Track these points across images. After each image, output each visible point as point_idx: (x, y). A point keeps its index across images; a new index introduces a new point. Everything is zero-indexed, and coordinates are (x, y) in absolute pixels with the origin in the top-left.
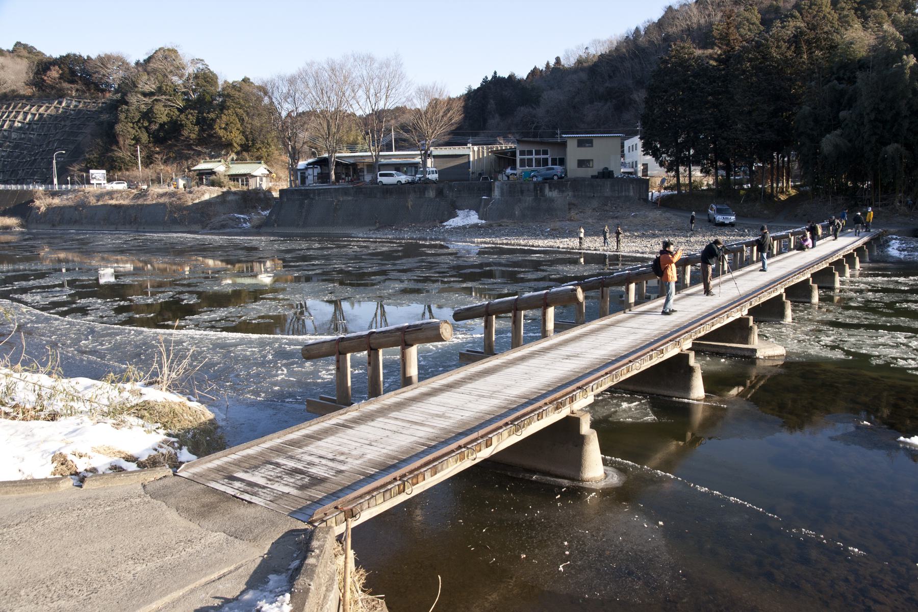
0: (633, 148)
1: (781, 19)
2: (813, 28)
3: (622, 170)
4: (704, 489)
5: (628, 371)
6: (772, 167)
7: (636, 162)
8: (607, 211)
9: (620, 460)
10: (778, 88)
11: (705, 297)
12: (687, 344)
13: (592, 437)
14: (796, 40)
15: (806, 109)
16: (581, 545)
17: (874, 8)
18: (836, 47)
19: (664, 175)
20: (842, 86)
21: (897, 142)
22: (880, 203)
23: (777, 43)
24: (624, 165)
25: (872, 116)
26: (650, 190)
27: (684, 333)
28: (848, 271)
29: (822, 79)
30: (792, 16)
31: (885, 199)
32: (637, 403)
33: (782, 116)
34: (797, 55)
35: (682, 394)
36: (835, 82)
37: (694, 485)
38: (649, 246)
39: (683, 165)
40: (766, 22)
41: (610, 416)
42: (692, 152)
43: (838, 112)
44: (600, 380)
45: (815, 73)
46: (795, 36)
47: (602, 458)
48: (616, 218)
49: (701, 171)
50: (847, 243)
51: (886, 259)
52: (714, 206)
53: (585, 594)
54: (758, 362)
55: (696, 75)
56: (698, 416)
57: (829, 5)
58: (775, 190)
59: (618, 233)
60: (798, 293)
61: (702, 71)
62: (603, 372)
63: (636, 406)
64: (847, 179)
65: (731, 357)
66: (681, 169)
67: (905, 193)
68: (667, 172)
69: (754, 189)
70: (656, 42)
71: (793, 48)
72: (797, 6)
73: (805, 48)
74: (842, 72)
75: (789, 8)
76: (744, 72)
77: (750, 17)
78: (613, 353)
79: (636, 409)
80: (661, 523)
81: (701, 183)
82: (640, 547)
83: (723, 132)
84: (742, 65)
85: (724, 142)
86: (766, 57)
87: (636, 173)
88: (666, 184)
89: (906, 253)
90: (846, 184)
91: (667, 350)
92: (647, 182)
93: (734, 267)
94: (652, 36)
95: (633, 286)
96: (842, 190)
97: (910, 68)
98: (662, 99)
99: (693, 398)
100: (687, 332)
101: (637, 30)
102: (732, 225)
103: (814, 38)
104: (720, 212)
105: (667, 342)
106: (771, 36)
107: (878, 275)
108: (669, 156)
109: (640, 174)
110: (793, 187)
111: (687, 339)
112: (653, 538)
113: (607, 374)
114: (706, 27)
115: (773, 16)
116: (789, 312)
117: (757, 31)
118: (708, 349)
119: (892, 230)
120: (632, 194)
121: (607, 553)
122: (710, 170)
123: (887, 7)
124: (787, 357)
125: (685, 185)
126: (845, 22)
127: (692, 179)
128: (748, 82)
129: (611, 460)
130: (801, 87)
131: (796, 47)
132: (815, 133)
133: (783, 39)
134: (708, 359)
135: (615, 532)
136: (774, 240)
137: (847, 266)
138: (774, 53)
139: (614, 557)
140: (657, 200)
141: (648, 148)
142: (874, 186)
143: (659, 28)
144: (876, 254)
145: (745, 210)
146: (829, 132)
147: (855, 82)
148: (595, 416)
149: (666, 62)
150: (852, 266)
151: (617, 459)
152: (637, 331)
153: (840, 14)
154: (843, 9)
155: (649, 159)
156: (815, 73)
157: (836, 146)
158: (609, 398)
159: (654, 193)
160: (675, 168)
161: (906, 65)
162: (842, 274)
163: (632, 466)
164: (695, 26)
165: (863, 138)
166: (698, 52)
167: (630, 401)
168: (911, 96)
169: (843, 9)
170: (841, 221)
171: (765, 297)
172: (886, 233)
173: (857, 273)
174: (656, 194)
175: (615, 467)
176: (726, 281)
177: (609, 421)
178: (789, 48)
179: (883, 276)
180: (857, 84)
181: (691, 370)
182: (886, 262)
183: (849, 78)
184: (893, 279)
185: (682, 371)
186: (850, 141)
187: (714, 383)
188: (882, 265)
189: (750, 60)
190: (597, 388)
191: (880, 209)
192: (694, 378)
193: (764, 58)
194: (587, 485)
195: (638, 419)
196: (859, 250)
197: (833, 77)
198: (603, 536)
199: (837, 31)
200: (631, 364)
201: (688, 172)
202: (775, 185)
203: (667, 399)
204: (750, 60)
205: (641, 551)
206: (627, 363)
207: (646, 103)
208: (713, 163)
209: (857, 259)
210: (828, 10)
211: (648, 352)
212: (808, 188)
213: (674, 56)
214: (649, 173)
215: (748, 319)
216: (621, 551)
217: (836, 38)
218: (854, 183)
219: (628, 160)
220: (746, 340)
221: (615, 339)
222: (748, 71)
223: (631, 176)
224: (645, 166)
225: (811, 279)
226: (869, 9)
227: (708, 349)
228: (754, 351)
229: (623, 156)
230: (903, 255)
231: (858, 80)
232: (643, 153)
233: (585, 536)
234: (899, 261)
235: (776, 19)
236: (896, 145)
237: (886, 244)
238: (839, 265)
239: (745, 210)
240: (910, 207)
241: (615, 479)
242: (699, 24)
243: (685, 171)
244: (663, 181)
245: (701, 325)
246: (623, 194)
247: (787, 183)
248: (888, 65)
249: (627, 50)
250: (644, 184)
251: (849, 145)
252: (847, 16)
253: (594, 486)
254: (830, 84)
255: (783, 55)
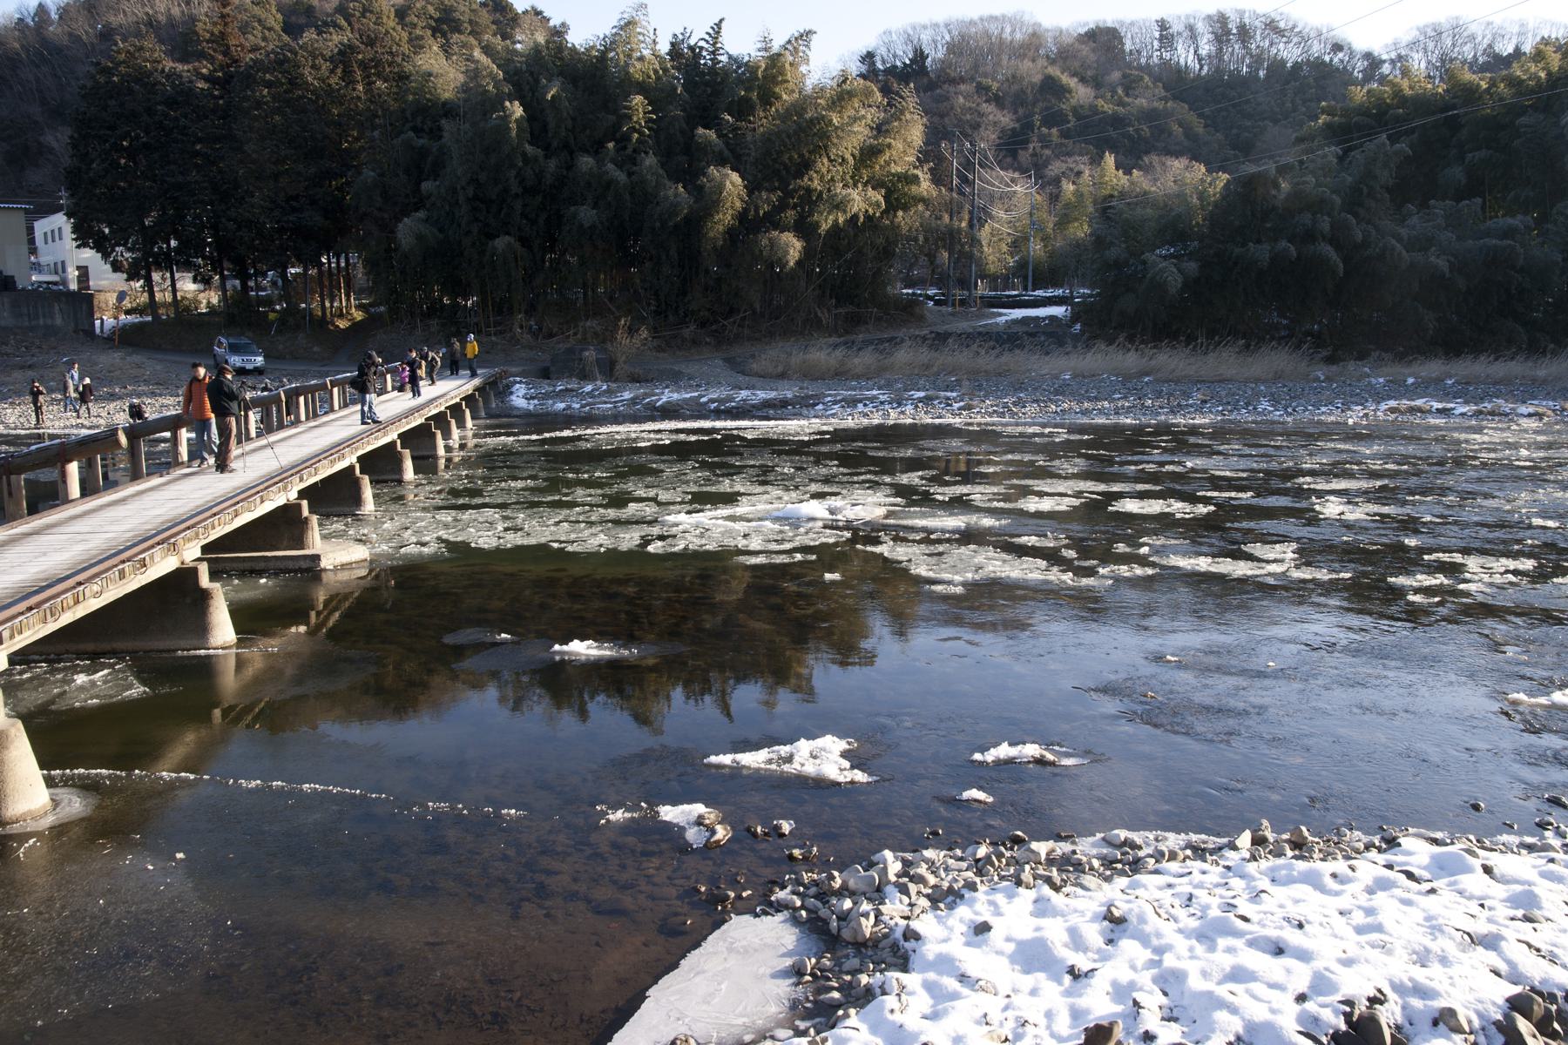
0: (55, 236)
1: (317, 27)
2: (371, 42)
3: (34, 278)
4: (253, 784)
5: (77, 602)
6: (320, 272)
7: (63, 263)
8: (7, 355)
9: (82, 771)
10: (319, 136)
11: (219, 475)
12: (191, 552)
13: (13, 731)
14: (344, 56)
15: (369, 174)
16: (15, 937)
17: (460, 32)
18: (407, 78)
19: (124, 286)
20: (421, 141)
21: (508, 233)
22: (492, 330)
23: (313, 61)
24: (37, 267)
25: (470, 192)
26: (97, 315)
27: (184, 530)
28: (456, 433)
29: (389, 128)
30: (335, 25)
31: (500, 324)
32: (106, 672)
33: (330, 186)
34: (348, 84)
35: (195, 642)
36: (411, 134)
37: (236, 782)
38: (104, 414)
39: (159, 267)
40: (291, 29)
41: (52, 702)
42: (173, 243)
43: (418, 184)
44: (17, 621)
45: (377, 116)
46: (341, 53)
47: (44, 777)
48: (30, 367)
49: (195, 281)
50: (447, 390)
51: (510, 412)
52: (223, 340)
53: (36, 1019)
54: (324, 575)
55: (171, 103)
56: (229, 681)
57: (392, 16)
58: (328, 311)
59: (36, 395)
60: (381, 464)
61: (182, 96)
62: (22, 606)
63: (106, 676)
64: (443, 293)
65: (276, 575)
66: (156, 276)
67: (526, 312)
68: (127, 280)
69: (292, 311)
70: (84, 37)
71: (339, 71)
72: (341, 10)
73: (358, 75)
74: (419, 119)
75: (330, 11)
76: (258, 104)
77: (263, 16)
78: (41, 576)
79: (105, 682)
80: (180, 856)
81: (197, 302)
82: (144, 906)
83: (229, 209)
84: (253, 91)
85: (231, 225)
86: (295, 82)
87: (64, 282)
88: (127, 304)
89: (536, 401)
90: (441, 300)
91: (152, 557)
92: (89, 299)
93: (267, 427)
94: (74, 26)
95: (73, 468)
96: (435, 309)
97: (516, 120)
98: (106, 141)
99: (214, 645)
100: (188, 528)
101: (42, 10)
102: (258, 371)
103: (372, 60)
104: (235, 349)
105: (152, 547)
106: (301, 47)
107: (500, 435)
108: (129, 250)
109: (73, 286)
110: (358, 307)
111: (190, 540)
112: (167, 885)
113: (30, 609)
114: (184, 23)
115: (302, 20)
116: (368, 492)
117: (277, 43)
118: (235, 565)
119: (514, 370)
120: (59, 321)
121: (76, 934)
122: (211, 278)
123: (477, 33)
124: (372, 562)
125: (164, 304)
126: (417, 44)
127: (179, 295)
128: (267, 123)
129: (64, 775)
130: (357, 139)
131: (344, 71)
132: (386, 216)
133: (323, 56)
134: (236, 581)
135: (89, 895)
136: (333, 386)
137: (453, 422)
138: (309, 75)
139: (91, 936)
140: (114, 333)
141: (85, 235)
142: (482, 303)
143: (89, 11)
144: (494, 405)
145: (281, 347)
146: (408, 216)
147: (441, 137)
148: (19, 709)
149: (107, 71)
150: (461, 425)
151: (76, 771)
152: (88, 536)
153: (410, 33)
154: (415, 26)
155: (89, 255)
156: (377, 116)
157: (420, 237)
158: (45, 673)
159: (106, 320)
160: (143, 272)
161: (510, 116)
162: (447, 435)
163: (109, 777)
164: (162, 19)
165: (459, 226)
166: (169, 65)
167: (90, 671)
168: (520, 164)
169: (415, 26)
170: (437, 353)
171: (326, 471)
172: (506, 374)
173: (470, 434)
174: (110, 322)
175: (73, 786)
176: (254, 451)
177: (52, 712)
178: (332, 71)
179: (508, 435)
180: (443, 140)
181: (204, 596)
182: (509, 416)
183: (431, 130)
184: (521, 438)
185: (188, 600)
186: (441, 230)
187: (249, 620)
188: (505, 420)
189: (269, 85)
190: (12, 637)
191: (493, 338)
192: (211, 609)
193: (292, 82)
194: (15, 829)
195: (111, 697)
196: (469, 399)
197: (408, 125)
198: (63, 907)
199: (406, 58)
200: (81, 588)
201: (168, 282)
202: (327, 304)
203: (165, 655)
204: (269, 85)
205: (147, 912)
206: (74, 588)
207: (75, 146)
208: (217, 267)
209: (468, 412)
210: (392, 24)
211: (116, 566)
212: (382, 309)
213: (124, 62)
214: (91, 283)
215: (299, 506)
216: (107, 922)
217: (408, 68)
218: (453, 299)
219: (46, 256)
220: (299, 542)
221: (45, 554)
222: (265, 103)
223: (55, 288)
224: (84, 272)
225: (399, 442)
226: (452, 32)
227: (235, 565)
228: (317, 558)
229: (33, 251)
230: (531, 406)
231: (445, 134)
232: (75, 244)
233: (21, 918)
234: (527, 414)
235: (308, 26)
236: (507, 238)
237: (507, 391)
238: (440, 419)
239: (281, 347)
240: (535, 335)
241: (75, 805)
242: (170, 16)
243: (164, 279)
244: (121, 296)
245: (215, 515)
246: (41, 322)
247: (348, 300)
248: (485, 115)
249: (22, 46)
250: (83, 301)
251: (441, 236)
252: (422, 38)
253: (31, 826)
254: (403, 136)
255: (324, 82)
